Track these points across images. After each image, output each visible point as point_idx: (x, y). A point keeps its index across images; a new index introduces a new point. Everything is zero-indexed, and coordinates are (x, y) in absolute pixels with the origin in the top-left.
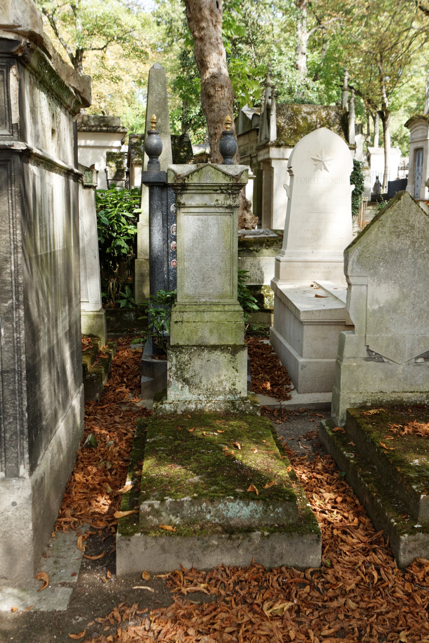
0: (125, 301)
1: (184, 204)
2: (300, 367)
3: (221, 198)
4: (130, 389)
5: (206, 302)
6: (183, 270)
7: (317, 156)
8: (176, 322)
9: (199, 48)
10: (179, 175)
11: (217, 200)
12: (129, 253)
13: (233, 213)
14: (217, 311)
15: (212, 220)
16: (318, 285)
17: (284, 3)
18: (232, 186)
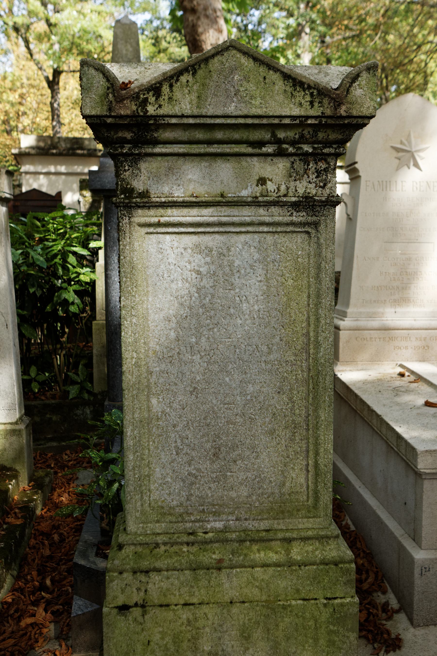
0: (77, 387)
1: (145, 194)
2: (417, 571)
3: (276, 172)
4: (53, 613)
5: (226, 530)
6: (146, 422)
7: (402, 143)
8: (124, 609)
9: (191, 24)
10: (125, 86)
11: (262, 181)
12: (83, 311)
13: (316, 225)
14: (265, 565)
15: (243, 248)
16: (413, 372)
17: (290, 4)
18: (316, 128)
